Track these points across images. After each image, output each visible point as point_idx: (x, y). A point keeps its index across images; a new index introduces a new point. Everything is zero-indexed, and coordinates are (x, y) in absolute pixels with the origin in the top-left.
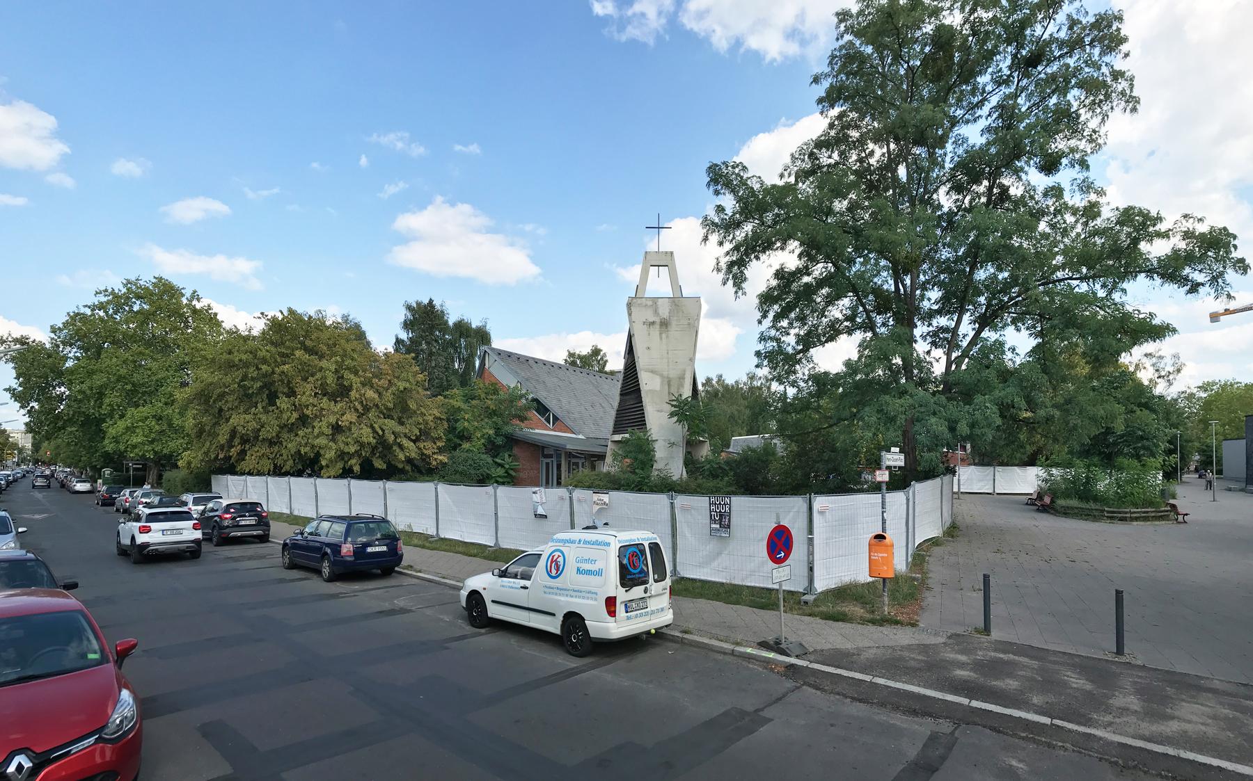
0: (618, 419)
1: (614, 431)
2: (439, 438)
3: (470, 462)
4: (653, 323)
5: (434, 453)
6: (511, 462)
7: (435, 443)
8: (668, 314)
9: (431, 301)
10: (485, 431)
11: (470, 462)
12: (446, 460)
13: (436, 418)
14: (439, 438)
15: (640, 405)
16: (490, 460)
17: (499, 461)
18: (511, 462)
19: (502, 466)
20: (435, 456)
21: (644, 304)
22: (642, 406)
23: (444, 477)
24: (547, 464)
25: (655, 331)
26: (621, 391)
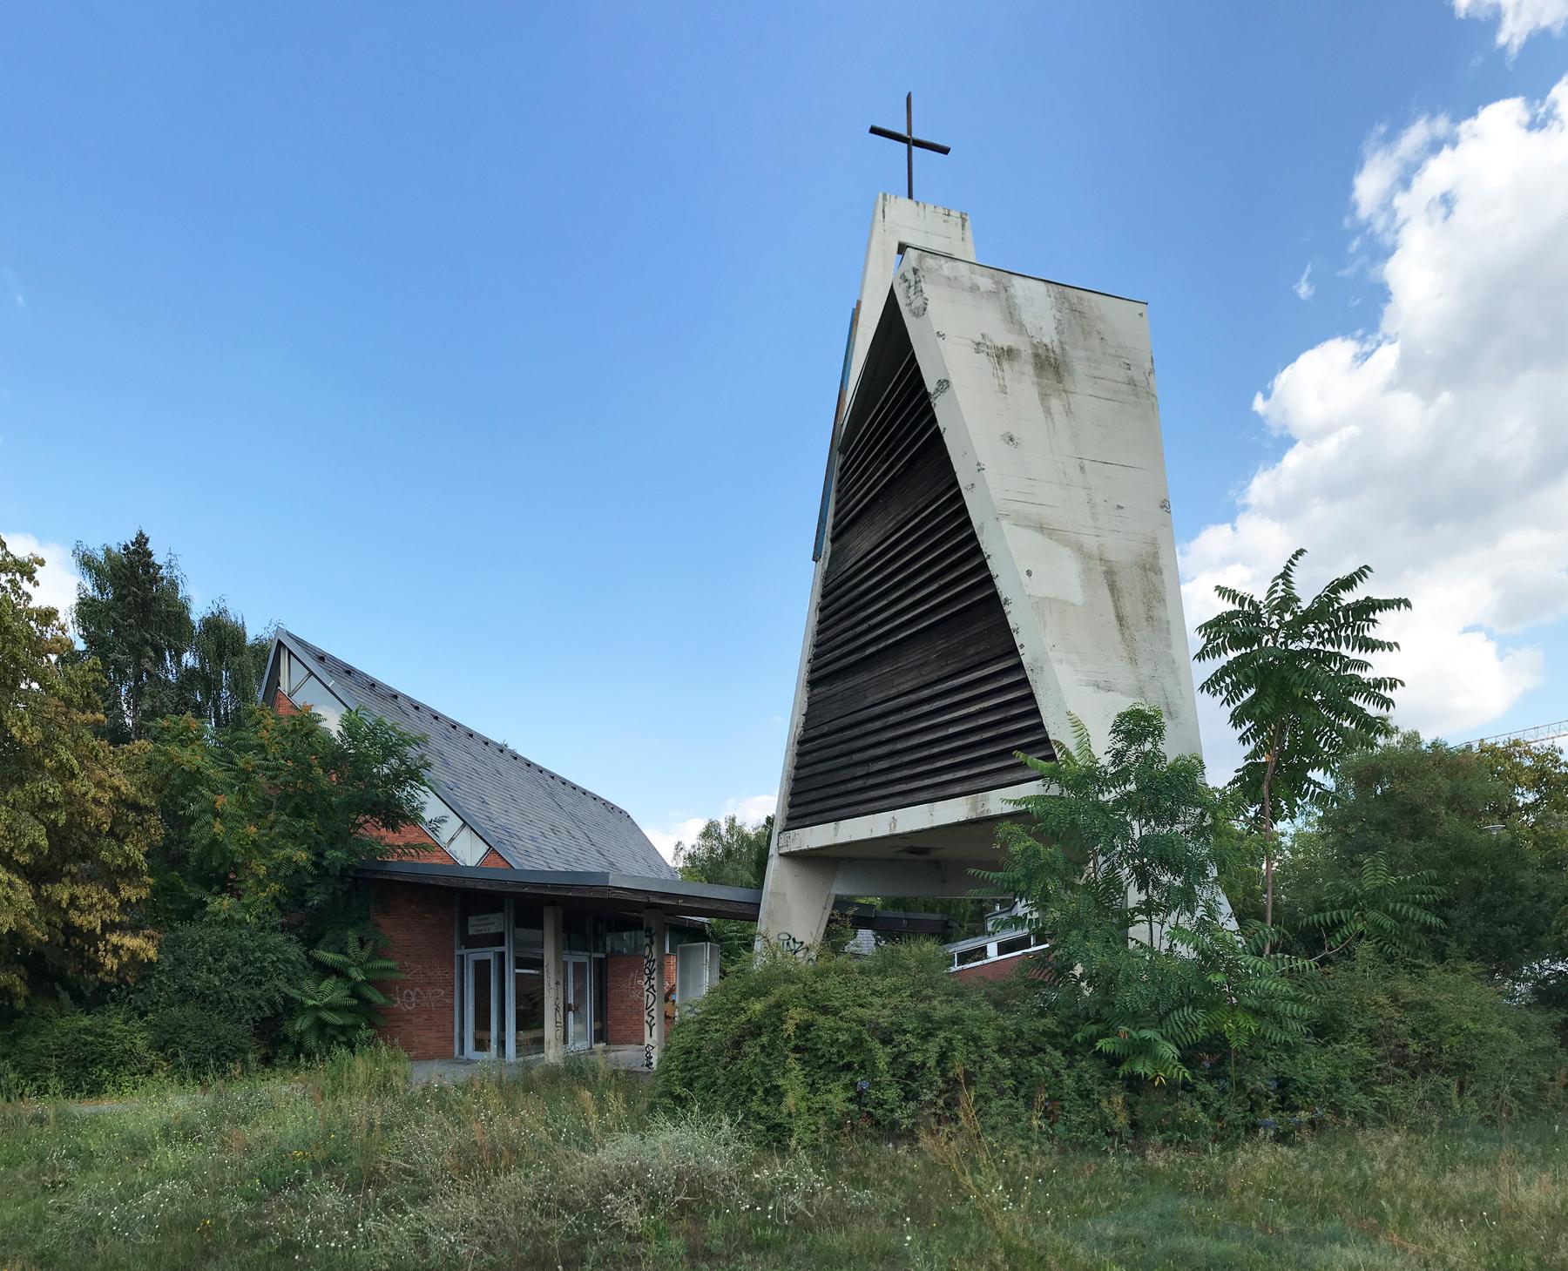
0: (804, 772)
1: (789, 819)
2: (130, 873)
3: (230, 958)
4: (1009, 354)
5: (109, 927)
6: (368, 960)
7: (115, 891)
8: (1055, 337)
9: (141, 541)
10: (279, 854)
11: (230, 958)
12: (152, 953)
13: (122, 801)
14: (130, 873)
15: (1017, 678)
16: (294, 952)
17: (329, 957)
18: (368, 960)
19: (338, 972)
20: (114, 938)
21: (967, 283)
22: (1019, 666)
23: (142, 1015)
24: (482, 969)
25: (1023, 381)
26: (812, 671)
